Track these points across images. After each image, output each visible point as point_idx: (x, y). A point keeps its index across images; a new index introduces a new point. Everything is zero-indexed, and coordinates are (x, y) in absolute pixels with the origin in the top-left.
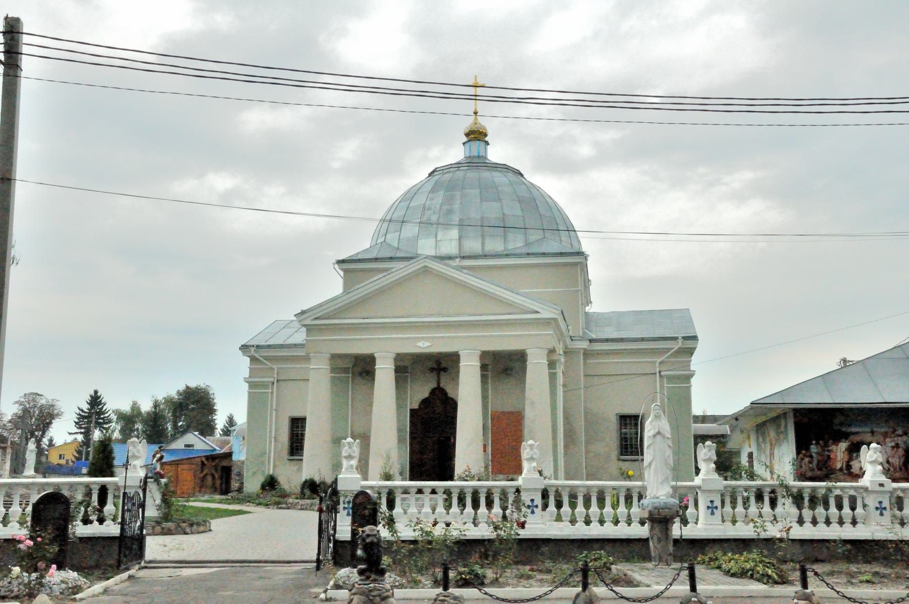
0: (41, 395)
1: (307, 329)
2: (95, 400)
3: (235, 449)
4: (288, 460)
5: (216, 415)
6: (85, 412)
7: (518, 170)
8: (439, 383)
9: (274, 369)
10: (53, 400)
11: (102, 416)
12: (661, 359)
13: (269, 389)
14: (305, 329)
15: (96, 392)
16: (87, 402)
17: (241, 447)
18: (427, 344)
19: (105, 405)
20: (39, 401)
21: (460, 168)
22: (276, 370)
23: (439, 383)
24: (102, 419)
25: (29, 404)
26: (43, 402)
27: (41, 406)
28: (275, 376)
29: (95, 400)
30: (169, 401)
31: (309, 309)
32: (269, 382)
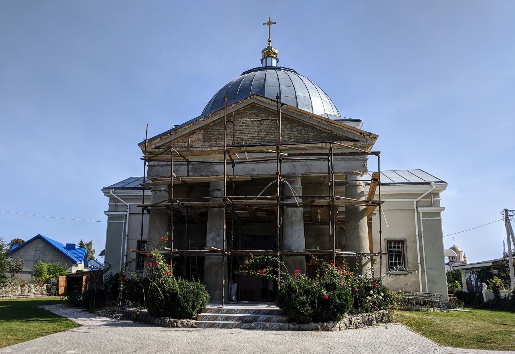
1: (110, 198)
7: (293, 70)
9: (127, 205)
12: (417, 200)
13: (123, 220)
14: (109, 198)
22: (129, 206)
28: (128, 210)
31: (511, 224)
32: (123, 215)
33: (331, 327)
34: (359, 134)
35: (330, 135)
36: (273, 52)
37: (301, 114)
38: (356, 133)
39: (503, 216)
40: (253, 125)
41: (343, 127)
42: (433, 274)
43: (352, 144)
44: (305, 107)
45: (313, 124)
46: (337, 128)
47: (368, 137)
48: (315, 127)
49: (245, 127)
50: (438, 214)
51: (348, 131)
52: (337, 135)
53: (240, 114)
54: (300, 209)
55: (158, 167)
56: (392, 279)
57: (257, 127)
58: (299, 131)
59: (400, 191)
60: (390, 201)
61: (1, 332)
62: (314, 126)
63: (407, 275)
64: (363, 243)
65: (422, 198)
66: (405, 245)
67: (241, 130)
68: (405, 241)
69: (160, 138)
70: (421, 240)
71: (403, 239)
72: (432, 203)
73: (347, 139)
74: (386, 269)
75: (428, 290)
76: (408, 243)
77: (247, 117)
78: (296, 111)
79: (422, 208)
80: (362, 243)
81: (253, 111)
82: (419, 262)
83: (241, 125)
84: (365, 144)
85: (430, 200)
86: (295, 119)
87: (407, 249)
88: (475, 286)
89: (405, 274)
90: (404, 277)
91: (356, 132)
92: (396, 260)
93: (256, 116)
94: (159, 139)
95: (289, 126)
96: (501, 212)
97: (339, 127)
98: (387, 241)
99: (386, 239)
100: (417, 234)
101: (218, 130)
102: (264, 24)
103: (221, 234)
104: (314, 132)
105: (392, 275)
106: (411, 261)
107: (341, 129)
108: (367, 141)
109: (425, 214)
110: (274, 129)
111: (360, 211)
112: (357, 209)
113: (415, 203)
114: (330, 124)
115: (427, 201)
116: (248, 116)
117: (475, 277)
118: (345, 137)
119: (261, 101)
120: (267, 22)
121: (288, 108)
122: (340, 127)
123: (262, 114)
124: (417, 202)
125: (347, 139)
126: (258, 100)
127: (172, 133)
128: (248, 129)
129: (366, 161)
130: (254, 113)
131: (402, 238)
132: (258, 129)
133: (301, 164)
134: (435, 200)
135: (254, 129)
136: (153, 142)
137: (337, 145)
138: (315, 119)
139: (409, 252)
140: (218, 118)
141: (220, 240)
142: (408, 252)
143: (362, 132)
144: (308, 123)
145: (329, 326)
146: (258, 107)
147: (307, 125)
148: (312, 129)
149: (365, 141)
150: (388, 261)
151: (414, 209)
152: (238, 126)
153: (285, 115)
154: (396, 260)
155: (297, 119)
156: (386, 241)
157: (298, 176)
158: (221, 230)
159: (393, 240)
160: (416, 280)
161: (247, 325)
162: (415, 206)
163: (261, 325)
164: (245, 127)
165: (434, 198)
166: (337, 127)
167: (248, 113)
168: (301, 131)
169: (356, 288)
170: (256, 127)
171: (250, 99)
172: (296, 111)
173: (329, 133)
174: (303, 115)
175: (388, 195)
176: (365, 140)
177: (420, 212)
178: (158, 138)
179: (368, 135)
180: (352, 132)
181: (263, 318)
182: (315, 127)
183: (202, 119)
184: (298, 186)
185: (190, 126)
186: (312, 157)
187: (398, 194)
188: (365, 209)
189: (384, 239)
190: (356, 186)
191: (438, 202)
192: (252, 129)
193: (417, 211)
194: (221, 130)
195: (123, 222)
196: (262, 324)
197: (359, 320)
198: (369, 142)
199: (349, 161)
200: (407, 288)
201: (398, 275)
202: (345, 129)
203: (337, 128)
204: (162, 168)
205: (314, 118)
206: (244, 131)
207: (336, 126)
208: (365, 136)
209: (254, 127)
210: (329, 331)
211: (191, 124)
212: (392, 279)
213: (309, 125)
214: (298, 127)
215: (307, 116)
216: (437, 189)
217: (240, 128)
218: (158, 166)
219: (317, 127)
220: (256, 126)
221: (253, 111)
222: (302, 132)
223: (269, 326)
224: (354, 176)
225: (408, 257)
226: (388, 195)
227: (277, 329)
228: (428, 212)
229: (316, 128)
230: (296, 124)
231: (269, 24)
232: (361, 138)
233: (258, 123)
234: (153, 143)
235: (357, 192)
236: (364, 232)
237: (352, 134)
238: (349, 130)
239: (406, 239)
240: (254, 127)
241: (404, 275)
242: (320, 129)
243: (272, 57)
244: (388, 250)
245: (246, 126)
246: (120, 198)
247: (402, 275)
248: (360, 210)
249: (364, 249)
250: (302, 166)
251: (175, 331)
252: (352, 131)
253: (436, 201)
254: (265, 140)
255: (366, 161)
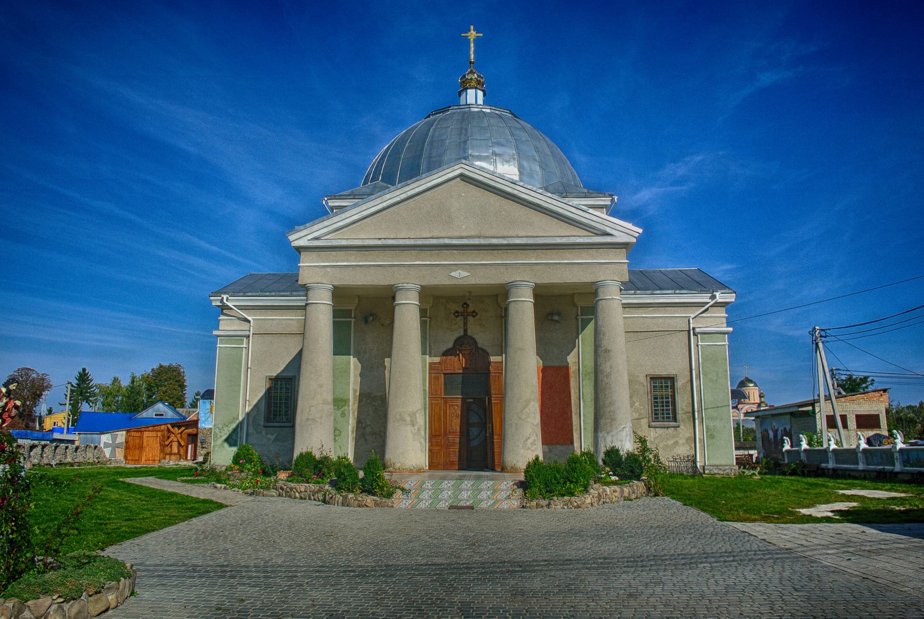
0: (33, 370)
2: (83, 377)
3: (202, 417)
4: (265, 427)
5: (185, 390)
6: (75, 387)
8: (465, 331)
9: (249, 321)
10: (43, 374)
11: (89, 391)
13: (243, 344)
15: (84, 370)
16: (76, 378)
17: (208, 415)
18: (465, 274)
19: (91, 381)
20: (31, 375)
21: (249, 367)
23: (465, 331)
24: (89, 393)
25: (22, 378)
26: (34, 376)
27: (32, 379)
29: (83, 377)
30: (145, 378)
39: (813, 338)
42: (714, 426)
61: (1, 483)
68: (675, 378)
88: (773, 442)
92: (663, 406)
96: (810, 332)
117: (773, 428)
150: (652, 407)
154: (663, 406)
156: (648, 378)
169: (202, 415)
186: (577, 247)
195: (243, 347)
244: (651, 392)
246: (239, 309)
251: (228, 506)
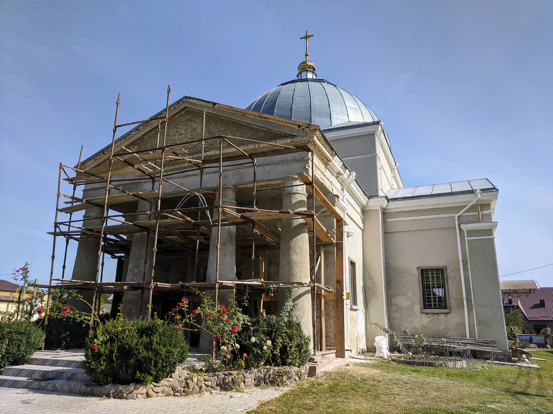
12: (459, 214)
33: (127, 393)
34: (297, 128)
35: (268, 134)
36: (308, 65)
37: (233, 112)
38: (293, 126)
40: (186, 132)
41: (279, 121)
43: (289, 141)
44: (321, 117)
45: (248, 124)
46: (272, 124)
47: (307, 129)
48: (251, 126)
49: (178, 137)
50: (490, 232)
51: (285, 125)
52: (275, 133)
53: (174, 122)
54: (226, 229)
55: (92, 192)
56: (429, 320)
57: (190, 135)
58: (233, 134)
59: (436, 205)
60: (424, 219)
62: (249, 125)
63: (448, 315)
64: (295, 270)
65: (465, 212)
66: (445, 274)
67: (174, 140)
69: (94, 159)
70: (467, 267)
71: (441, 266)
72: (479, 217)
73: (285, 136)
74: (420, 307)
75: (478, 335)
76: (449, 272)
77: (181, 125)
78: (228, 109)
79: (465, 225)
80: (293, 270)
81: (187, 117)
82: (465, 297)
83: (174, 134)
84: (305, 139)
85: (477, 213)
86: (230, 120)
87: (447, 280)
89: (446, 314)
90: (445, 317)
91: (293, 125)
93: (190, 123)
94: (93, 160)
95: (223, 129)
97: (274, 121)
98: (421, 270)
99: (420, 267)
100: (461, 259)
101: (152, 144)
102: (301, 38)
103: (140, 264)
104: (249, 133)
105: (428, 315)
106: (453, 295)
107: (277, 124)
108: (307, 135)
109: (471, 233)
110: (207, 135)
111: (294, 227)
112: (290, 224)
113: (456, 219)
114: (264, 119)
115: (474, 215)
116: (182, 124)
118: (284, 134)
119: (192, 103)
120: (304, 36)
121: (220, 107)
122: (276, 122)
123: (196, 119)
124: (459, 217)
125: (286, 136)
126: (190, 103)
127: (105, 152)
128: (180, 138)
129: (307, 162)
130: (188, 119)
131: (441, 265)
132: (191, 136)
133: (233, 173)
134: (485, 213)
135: (187, 137)
136: (86, 164)
137: (267, 145)
138: (248, 116)
139: (451, 283)
140: (150, 129)
141: (138, 272)
142: (449, 284)
143: (300, 124)
144: (243, 122)
145: (124, 391)
146: (193, 111)
147: (242, 125)
148: (248, 129)
149: (304, 136)
151: (456, 227)
152: (172, 136)
153: (219, 117)
155: (232, 119)
156: (420, 270)
157: (228, 188)
158: (141, 260)
159: (430, 268)
160: (460, 321)
161: (37, 385)
162: (457, 223)
163: (51, 385)
164: (178, 137)
165: (482, 211)
166: (272, 122)
167: (183, 120)
168: (235, 134)
170: (189, 135)
171: (183, 103)
172: (228, 109)
173: (266, 132)
174: (235, 114)
175: (421, 211)
176: (304, 134)
177: (464, 230)
178: (91, 159)
179: (307, 127)
180: (289, 127)
181: (67, 375)
182: (251, 126)
183: (134, 133)
184: (227, 201)
185: (122, 142)
187: (433, 209)
188: (114, 206)
189: (418, 267)
190: (291, 194)
191: (489, 216)
192: (185, 137)
193: (460, 230)
194: (154, 143)
196: (52, 383)
197: (210, 382)
198: (309, 136)
199: (287, 163)
200: (449, 332)
201: (436, 314)
202: (281, 123)
203: (272, 124)
204: (95, 192)
205: (247, 115)
206: (176, 141)
207: (271, 121)
208: (304, 129)
209: (187, 135)
210: (123, 399)
211: (123, 140)
212: (429, 320)
213: (244, 125)
214: (232, 129)
215: (240, 113)
216: (486, 198)
217: (173, 138)
218: (92, 189)
219: (253, 126)
220: (189, 133)
221: (187, 117)
222: (236, 134)
223: (59, 387)
224: (290, 182)
225: (450, 290)
226: (421, 211)
227: (66, 392)
228: (475, 230)
229: (252, 127)
230: (231, 126)
231: (306, 37)
232: (300, 132)
233: (192, 130)
234: (88, 165)
235: (291, 202)
236: (298, 254)
237: (289, 128)
238: (286, 124)
239: (446, 267)
240: (187, 135)
241: (444, 315)
242: (256, 127)
243: (307, 71)
245: (180, 135)
247: (442, 315)
248: (294, 226)
249: (295, 278)
250: (234, 175)
252: (289, 125)
253: (485, 214)
254: (196, 148)
255: (307, 162)
